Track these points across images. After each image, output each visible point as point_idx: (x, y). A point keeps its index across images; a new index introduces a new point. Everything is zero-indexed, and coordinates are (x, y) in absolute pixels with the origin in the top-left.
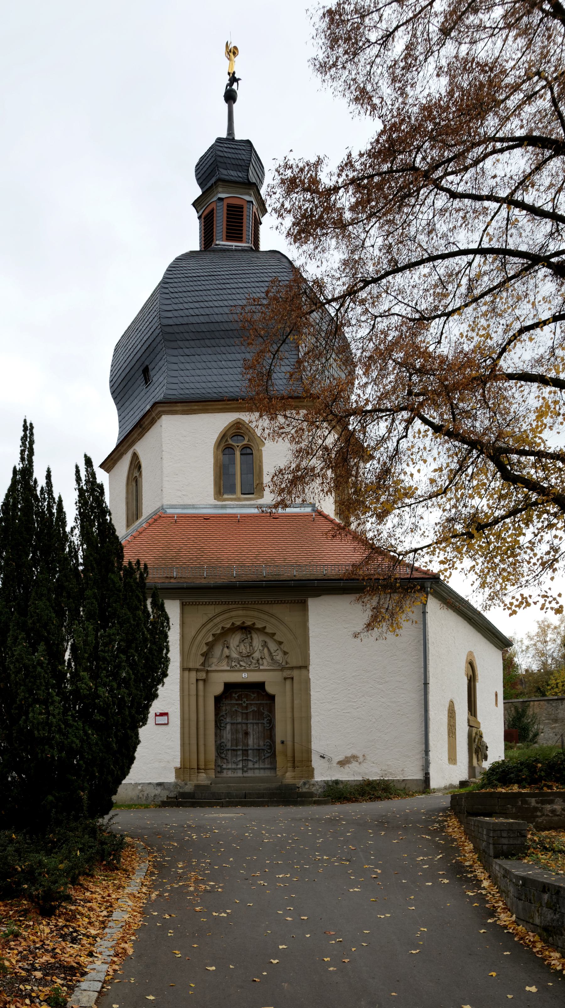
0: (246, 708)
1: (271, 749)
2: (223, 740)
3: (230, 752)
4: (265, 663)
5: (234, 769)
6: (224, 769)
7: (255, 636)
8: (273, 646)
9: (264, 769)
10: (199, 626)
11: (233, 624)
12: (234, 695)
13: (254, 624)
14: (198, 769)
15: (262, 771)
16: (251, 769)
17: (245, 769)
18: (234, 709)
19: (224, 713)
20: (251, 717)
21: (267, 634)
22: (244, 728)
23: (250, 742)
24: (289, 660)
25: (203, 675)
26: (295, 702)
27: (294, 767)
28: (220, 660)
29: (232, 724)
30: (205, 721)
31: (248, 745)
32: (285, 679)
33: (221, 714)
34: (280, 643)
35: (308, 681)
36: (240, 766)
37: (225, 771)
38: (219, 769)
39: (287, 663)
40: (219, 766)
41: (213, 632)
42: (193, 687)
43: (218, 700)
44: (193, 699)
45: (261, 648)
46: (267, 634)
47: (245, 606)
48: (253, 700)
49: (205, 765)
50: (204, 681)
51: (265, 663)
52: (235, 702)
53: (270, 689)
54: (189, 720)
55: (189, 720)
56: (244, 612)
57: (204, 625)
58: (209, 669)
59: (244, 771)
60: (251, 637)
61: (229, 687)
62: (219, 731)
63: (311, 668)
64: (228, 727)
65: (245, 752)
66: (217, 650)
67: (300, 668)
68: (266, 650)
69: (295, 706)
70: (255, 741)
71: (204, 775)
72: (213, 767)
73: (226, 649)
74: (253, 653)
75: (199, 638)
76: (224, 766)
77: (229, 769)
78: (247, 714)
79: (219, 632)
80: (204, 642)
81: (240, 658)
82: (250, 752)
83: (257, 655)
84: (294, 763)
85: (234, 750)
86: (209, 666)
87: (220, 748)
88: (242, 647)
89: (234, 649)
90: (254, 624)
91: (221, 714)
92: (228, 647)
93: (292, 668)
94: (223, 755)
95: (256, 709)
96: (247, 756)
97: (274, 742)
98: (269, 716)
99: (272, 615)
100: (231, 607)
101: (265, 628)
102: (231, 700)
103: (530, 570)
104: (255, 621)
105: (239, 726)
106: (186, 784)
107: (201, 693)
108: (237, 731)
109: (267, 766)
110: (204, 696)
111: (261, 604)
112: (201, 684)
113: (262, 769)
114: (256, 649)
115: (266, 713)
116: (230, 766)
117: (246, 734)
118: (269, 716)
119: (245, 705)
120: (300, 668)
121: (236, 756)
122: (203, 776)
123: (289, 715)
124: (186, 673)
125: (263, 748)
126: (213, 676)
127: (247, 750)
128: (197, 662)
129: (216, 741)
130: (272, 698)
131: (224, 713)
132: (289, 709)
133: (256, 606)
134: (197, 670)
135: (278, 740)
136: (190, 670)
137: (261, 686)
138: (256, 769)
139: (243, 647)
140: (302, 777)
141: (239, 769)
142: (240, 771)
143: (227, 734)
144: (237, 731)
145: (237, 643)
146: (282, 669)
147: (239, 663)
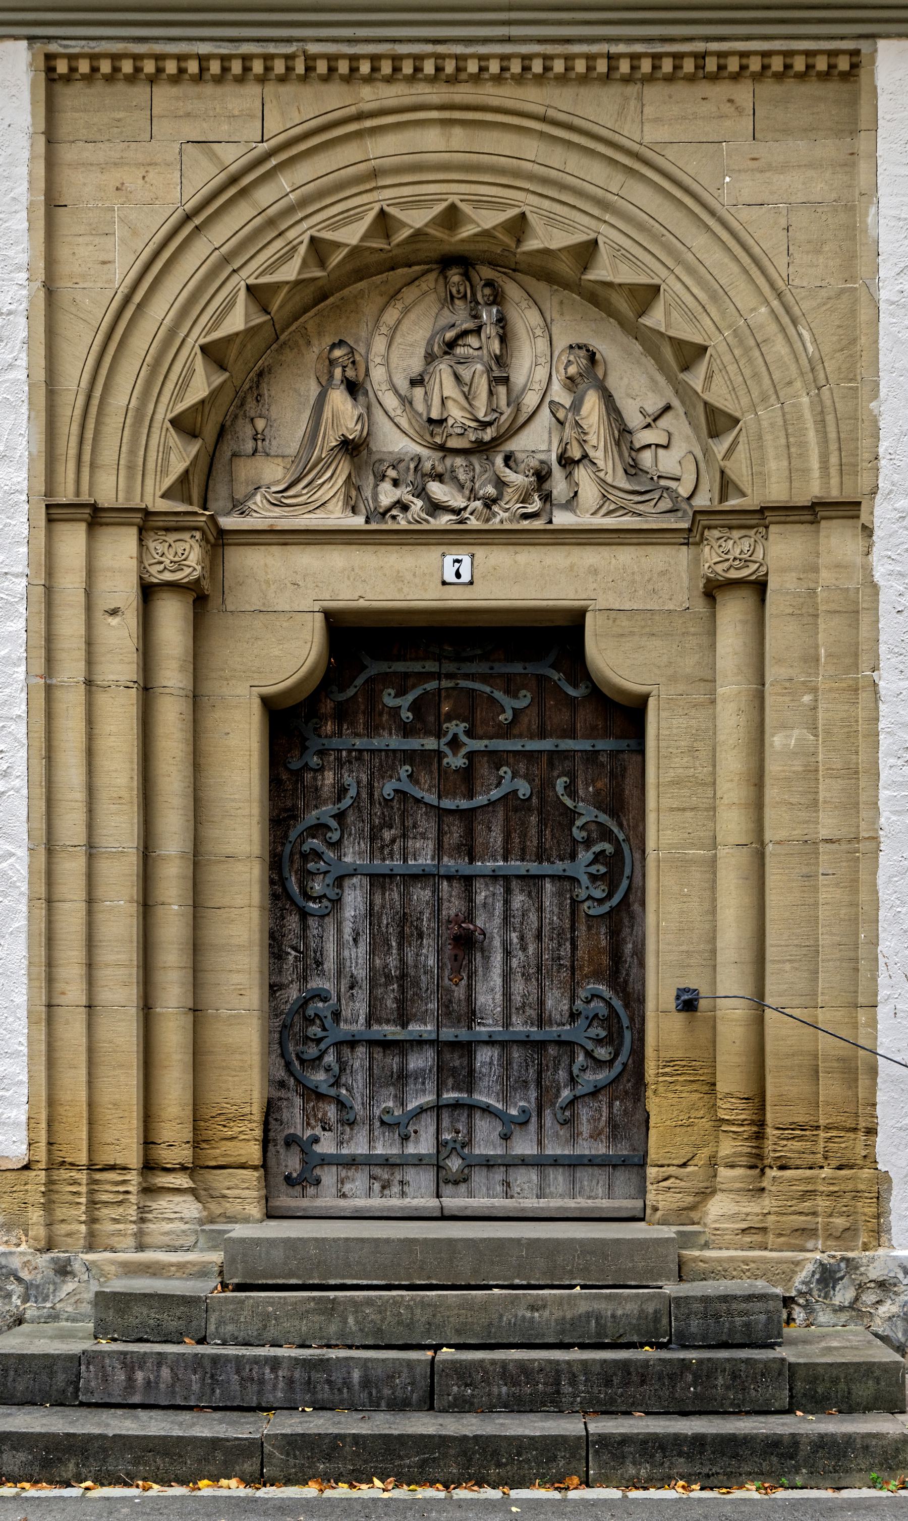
0: (467, 779)
1: (613, 1039)
2: (316, 983)
3: (359, 1058)
4: (589, 492)
5: (387, 1163)
6: (325, 1161)
7: (525, 319)
8: (637, 387)
9: (573, 1164)
10: (155, 223)
11: (384, 222)
12: (389, 700)
13: (519, 226)
14: (149, 1166)
15: (558, 1179)
16: (488, 1164)
17: (454, 1164)
18: (388, 789)
19: (325, 812)
20: (496, 838)
21: (597, 298)
22: (453, 906)
23: (489, 996)
24: (739, 469)
25: (184, 556)
26: (776, 741)
27: (757, 1163)
28: (303, 473)
29: (378, 881)
30: (198, 859)
31: (471, 1015)
32: (713, 590)
33: (312, 817)
34: (690, 354)
35: (859, 604)
36: (424, 1145)
37: (329, 1176)
38: (292, 1163)
39: (726, 485)
40: (291, 1141)
41: (249, 275)
42: (119, 635)
43: (287, 723)
44: (119, 714)
45: (559, 394)
46: (597, 298)
47: (463, 93)
48: (505, 732)
49: (198, 1142)
50: (201, 599)
51: (589, 492)
52: (395, 742)
53: (613, 659)
54: (91, 849)
55: (91, 849)
56: (459, 138)
57: (193, 221)
58: (228, 522)
59: (445, 1180)
60: (502, 321)
61: (352, 638)
62: (293, 922)
63: (882, 514)
64: (354, 900)
65: (456, 1060)
66: (292, 412)
67: (814, 513)
68: (592, 402)
69: (773, 767)
70: (519, 987)
71: (189, 1208)
72: (252, 1151)
73: (338, 398)
74: (514, 430)
75: (161, 309)
76: (327, 1146)
77: (352, 1162)
78: (467, 816)
79: (290, 272)
80: (197, 337)
81: (430, 460)
82: (484, 1056)
83: (537, 441)
84: (759, 1136)
85: (386, 1045)
86: (239, 506)
87: (296, 1031)
88: (444, 381)
89: (391, 402)
90: (519, 226)
91: (312, 817)
92: (353, 388)
93: (762, 517)
94: (319, 1077)
95: (524, 789)
96: (469, 1081)
97: (634, 1000)
98: (606, 834)
99: (636, 162)
100: (370, 96)
101: (587, 251)
102: (373, 729)
103: (890, 652)
104: (528, 203)
105: (422, 895)
106: (63, 1270)
107: (172, 676)
108: (407, 928)
109: (586, 1148)
110: (197, 700)
111: (563, 79)
112: (172, 616)
113: (556, 1162)
114: (531, 400)
115: (588, 813)
116: (359, 1146)
117: (465, 944)
118: (606, 834)
119: (456, 761)
120: (814, 513)
121: (401, 1078)
122: (178, 1211)
123: (732, 824)
124: (73, 540)
125: (566, 1031)
126: (256, 566)
127: (467, 1048)
128: (146, 467)
129: (274, 989)
130: (627, 716)
131: (325, 812)
132: (731, 790)
133: (532, 98)
134: (147, 523)
135: (659, 993)
136: (96, 517)
137: (555, 638)
138: (524, 1162)
139: (450, 389)
140: (808, 1232)
141: (419, 1161)
142: (423, 1179)
143: (345, 945)
144: (407, 928)
145: (416, 365)
146: (695, 530)
147: (421, 492)
